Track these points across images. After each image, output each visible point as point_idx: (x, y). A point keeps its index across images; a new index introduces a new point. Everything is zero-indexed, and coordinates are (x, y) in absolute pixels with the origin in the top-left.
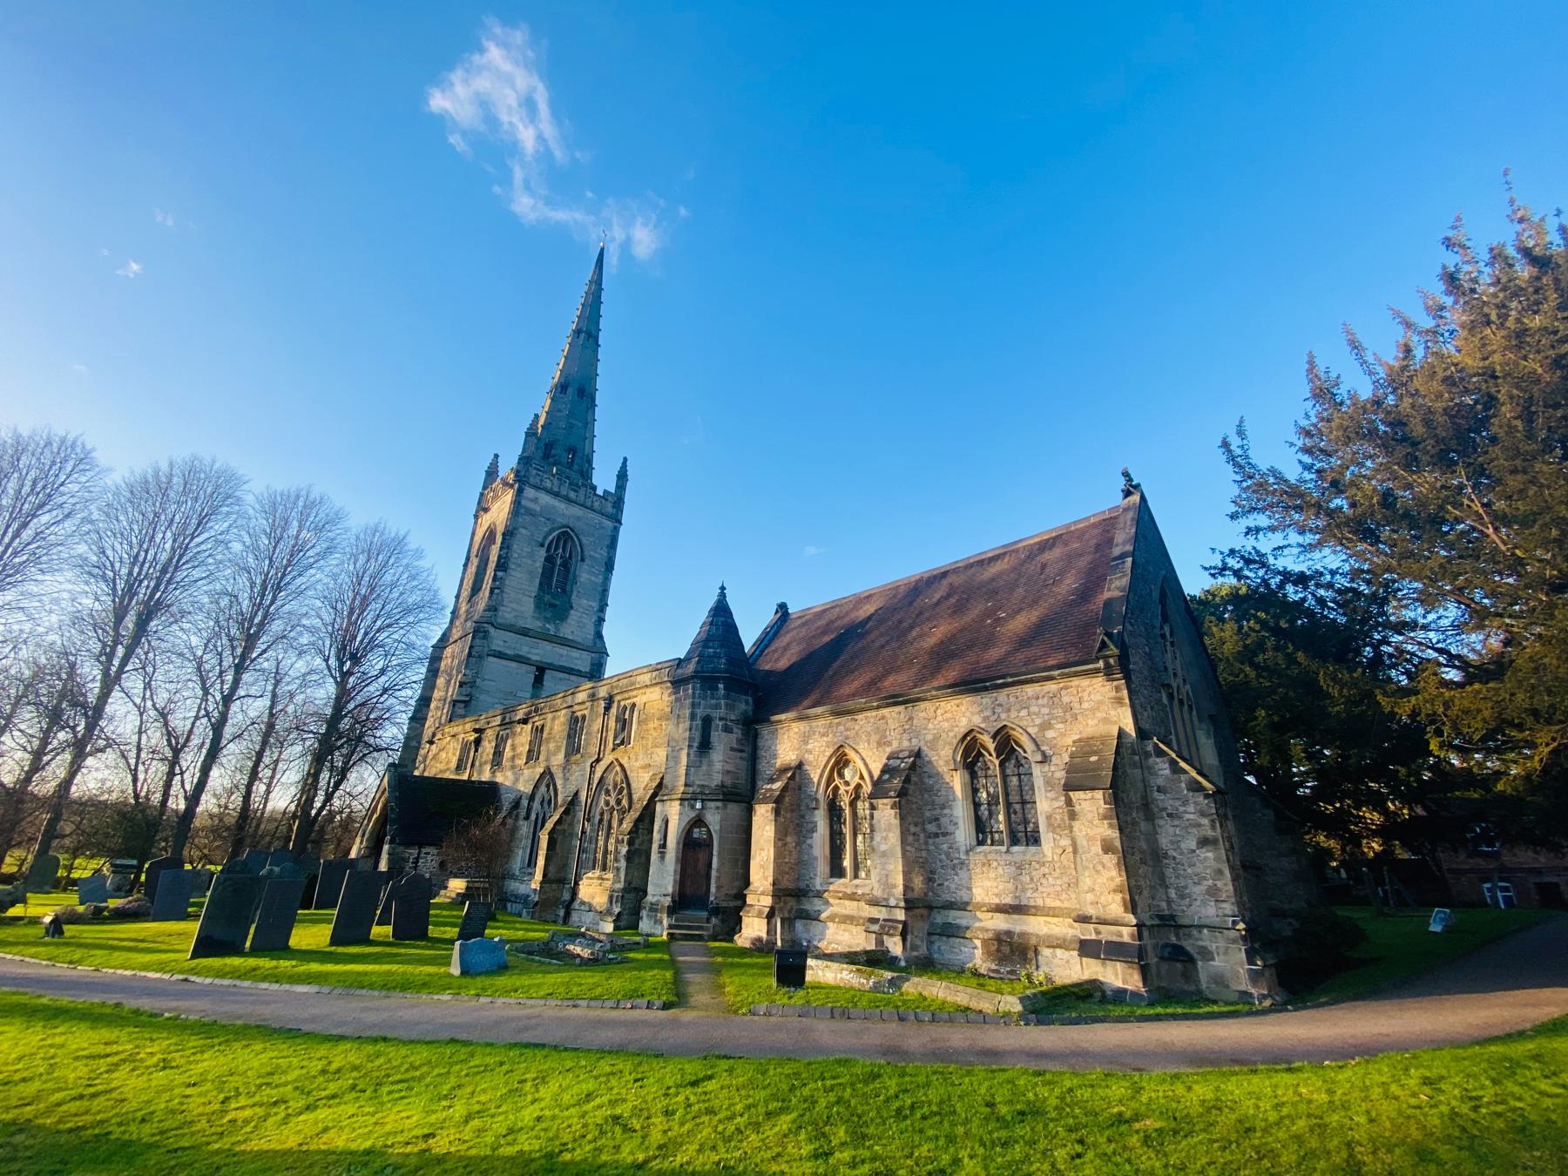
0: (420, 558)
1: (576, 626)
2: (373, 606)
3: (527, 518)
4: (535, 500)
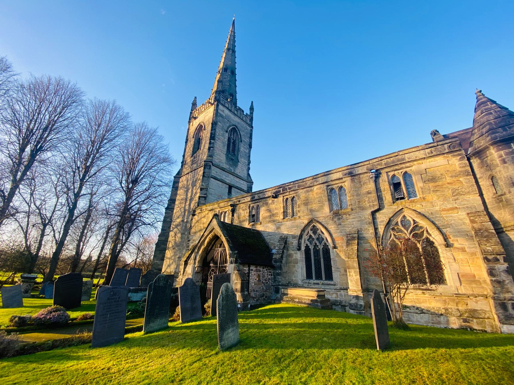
0: (162, 140)
1: (240, 170)
3: (221, 118)
4: (223, 111)
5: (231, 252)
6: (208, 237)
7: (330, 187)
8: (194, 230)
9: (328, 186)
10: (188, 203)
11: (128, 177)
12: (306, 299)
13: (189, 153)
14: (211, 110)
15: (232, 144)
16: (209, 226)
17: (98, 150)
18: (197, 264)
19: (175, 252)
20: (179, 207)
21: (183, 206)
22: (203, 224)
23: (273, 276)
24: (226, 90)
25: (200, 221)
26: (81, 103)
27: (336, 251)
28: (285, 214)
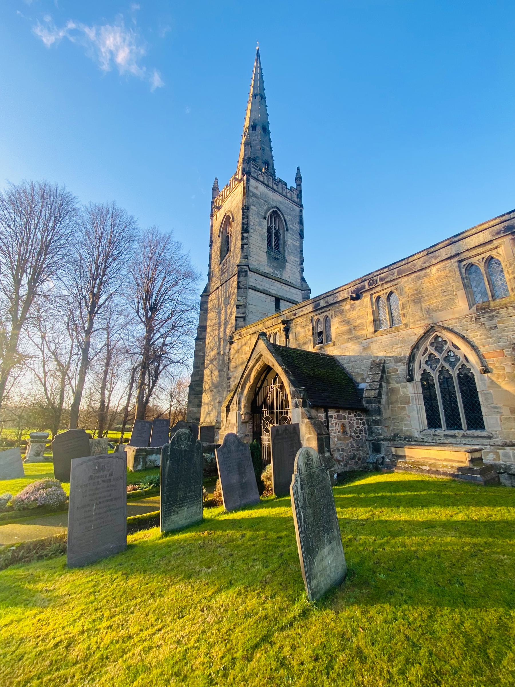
2: (159, 278)
3: (254, 199)
4: (256, 188)
5: (294, 389)
6: (255, 369)
7: (464, 263)
8: (234, 364)
9: (460, 261)
10: (223, 329)
11: (145, 304)
12: (447, 466)
13: (217, 260)
14: (240, 189)
15: (273, 236)
16: (254, 352)
17: (104, 272)
18: (242, 409)
19: (213, 396)
20: (211, 336)
21: (217, 333)
22: (246, 354)
23: (366, 426)
24: (257, 157)
25: (240, 351)
26: (75, 212)
27: (489, 378)
28: (377, 323)
